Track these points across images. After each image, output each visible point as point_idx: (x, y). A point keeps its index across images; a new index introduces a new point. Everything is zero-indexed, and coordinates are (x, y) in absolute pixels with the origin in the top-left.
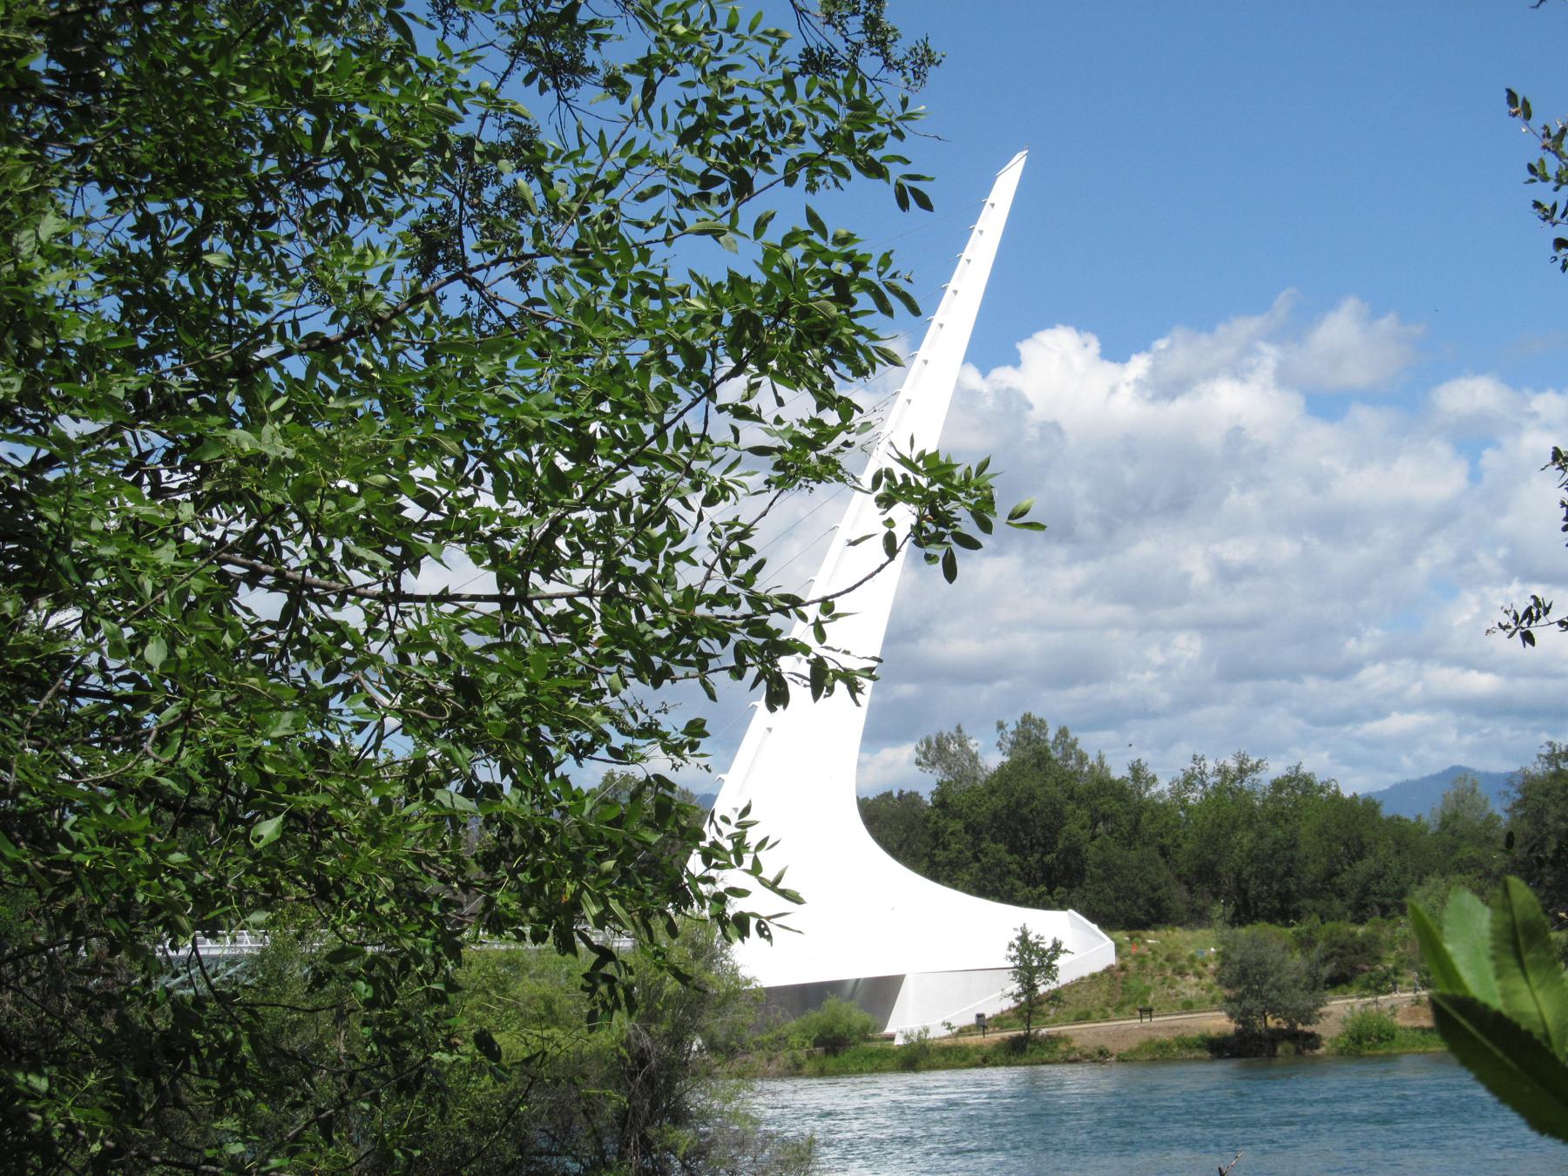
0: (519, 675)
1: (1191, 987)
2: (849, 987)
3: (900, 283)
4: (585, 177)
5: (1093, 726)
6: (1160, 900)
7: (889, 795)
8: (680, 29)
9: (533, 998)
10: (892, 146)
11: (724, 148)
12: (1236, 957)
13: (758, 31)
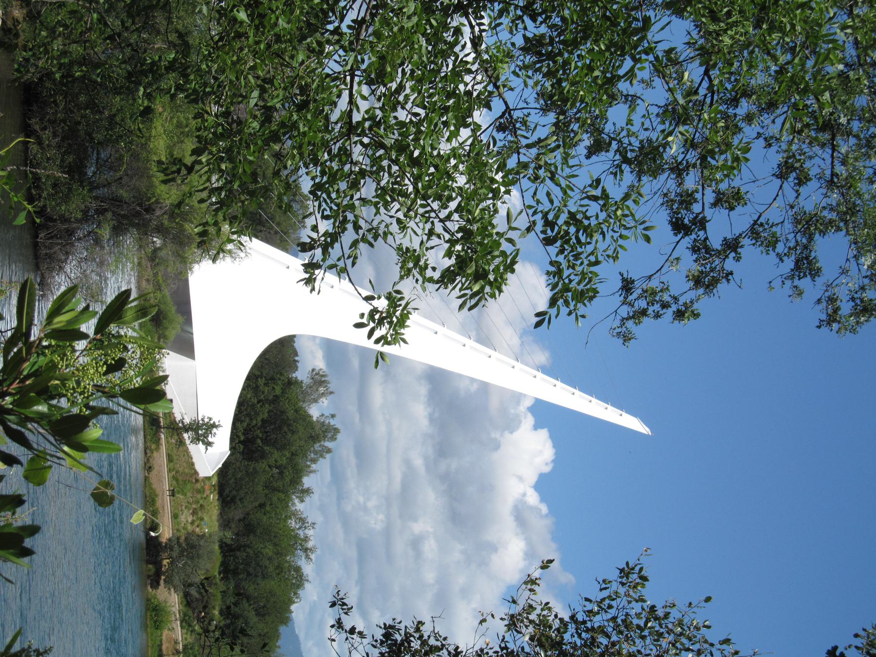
0: (310, 128)
1: (186, 518)
2: (188, 329)
3: (483, 302)
4: (556, 168)
5: (333, 467)
6: (235, 503)
7: (297, 355)
8: (619, 213)
9: (183, 151)
10: (564, 310)
11: (567, 233)
12: (202, 542)
13: (618, 248)
